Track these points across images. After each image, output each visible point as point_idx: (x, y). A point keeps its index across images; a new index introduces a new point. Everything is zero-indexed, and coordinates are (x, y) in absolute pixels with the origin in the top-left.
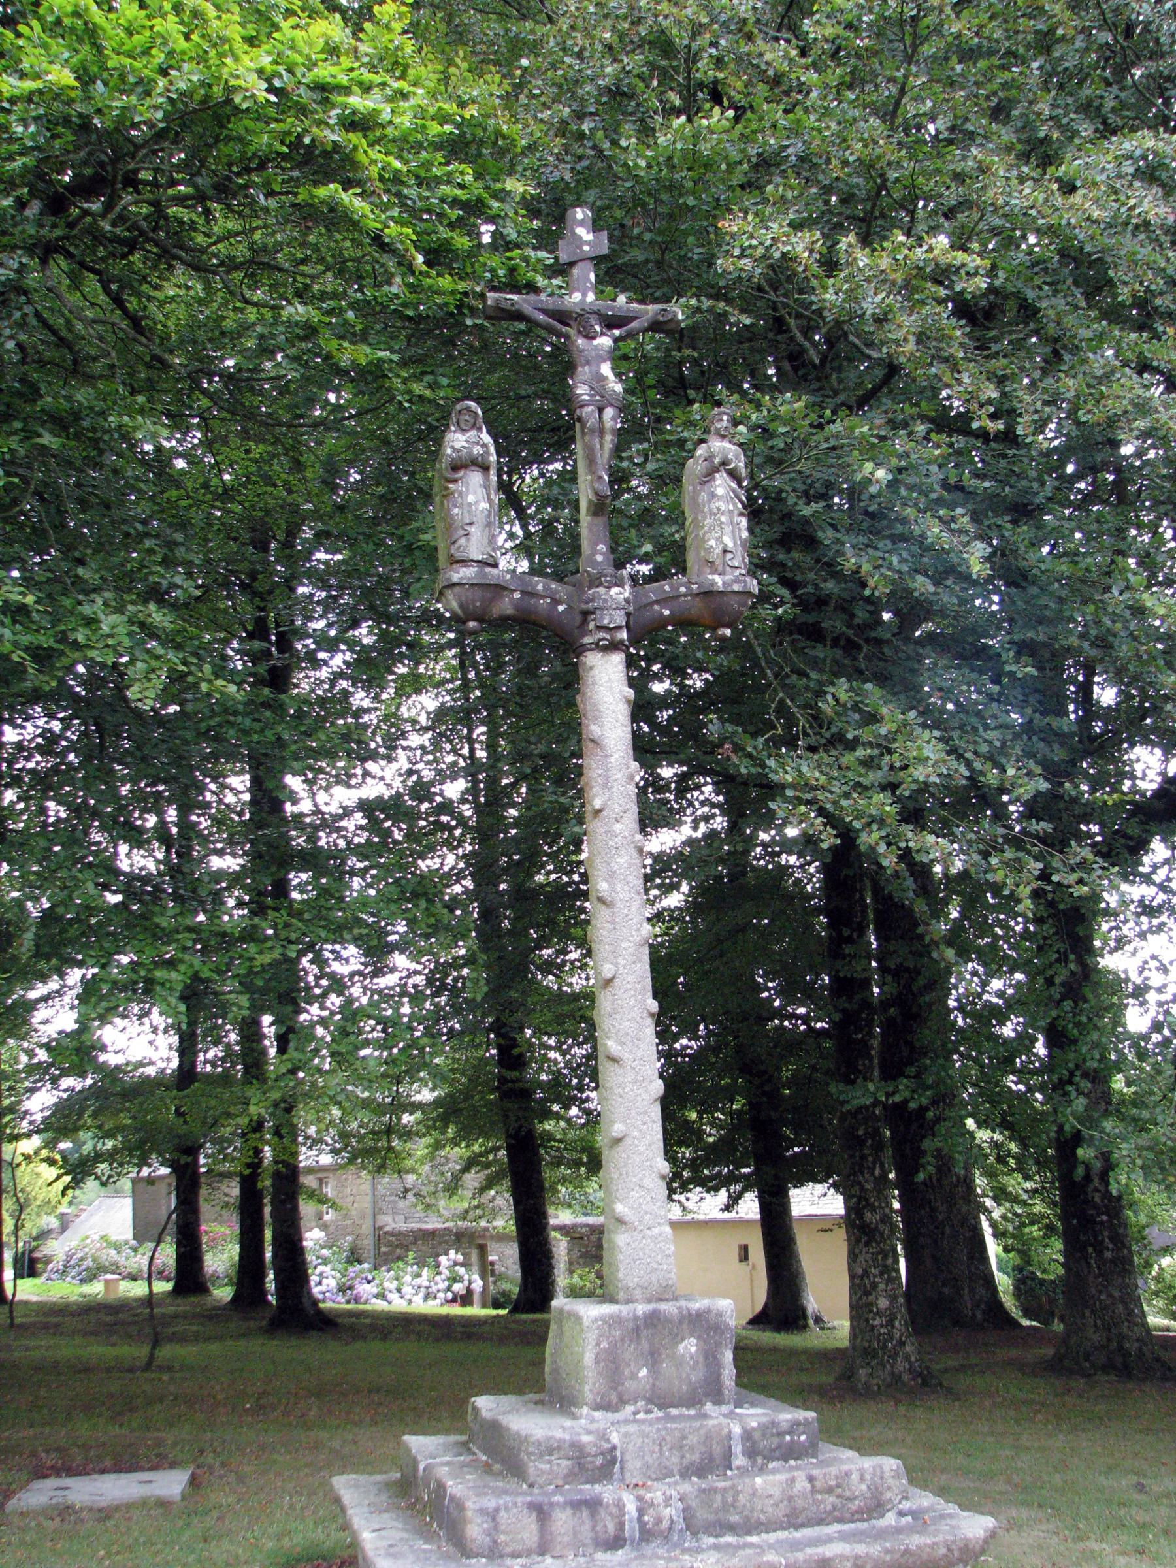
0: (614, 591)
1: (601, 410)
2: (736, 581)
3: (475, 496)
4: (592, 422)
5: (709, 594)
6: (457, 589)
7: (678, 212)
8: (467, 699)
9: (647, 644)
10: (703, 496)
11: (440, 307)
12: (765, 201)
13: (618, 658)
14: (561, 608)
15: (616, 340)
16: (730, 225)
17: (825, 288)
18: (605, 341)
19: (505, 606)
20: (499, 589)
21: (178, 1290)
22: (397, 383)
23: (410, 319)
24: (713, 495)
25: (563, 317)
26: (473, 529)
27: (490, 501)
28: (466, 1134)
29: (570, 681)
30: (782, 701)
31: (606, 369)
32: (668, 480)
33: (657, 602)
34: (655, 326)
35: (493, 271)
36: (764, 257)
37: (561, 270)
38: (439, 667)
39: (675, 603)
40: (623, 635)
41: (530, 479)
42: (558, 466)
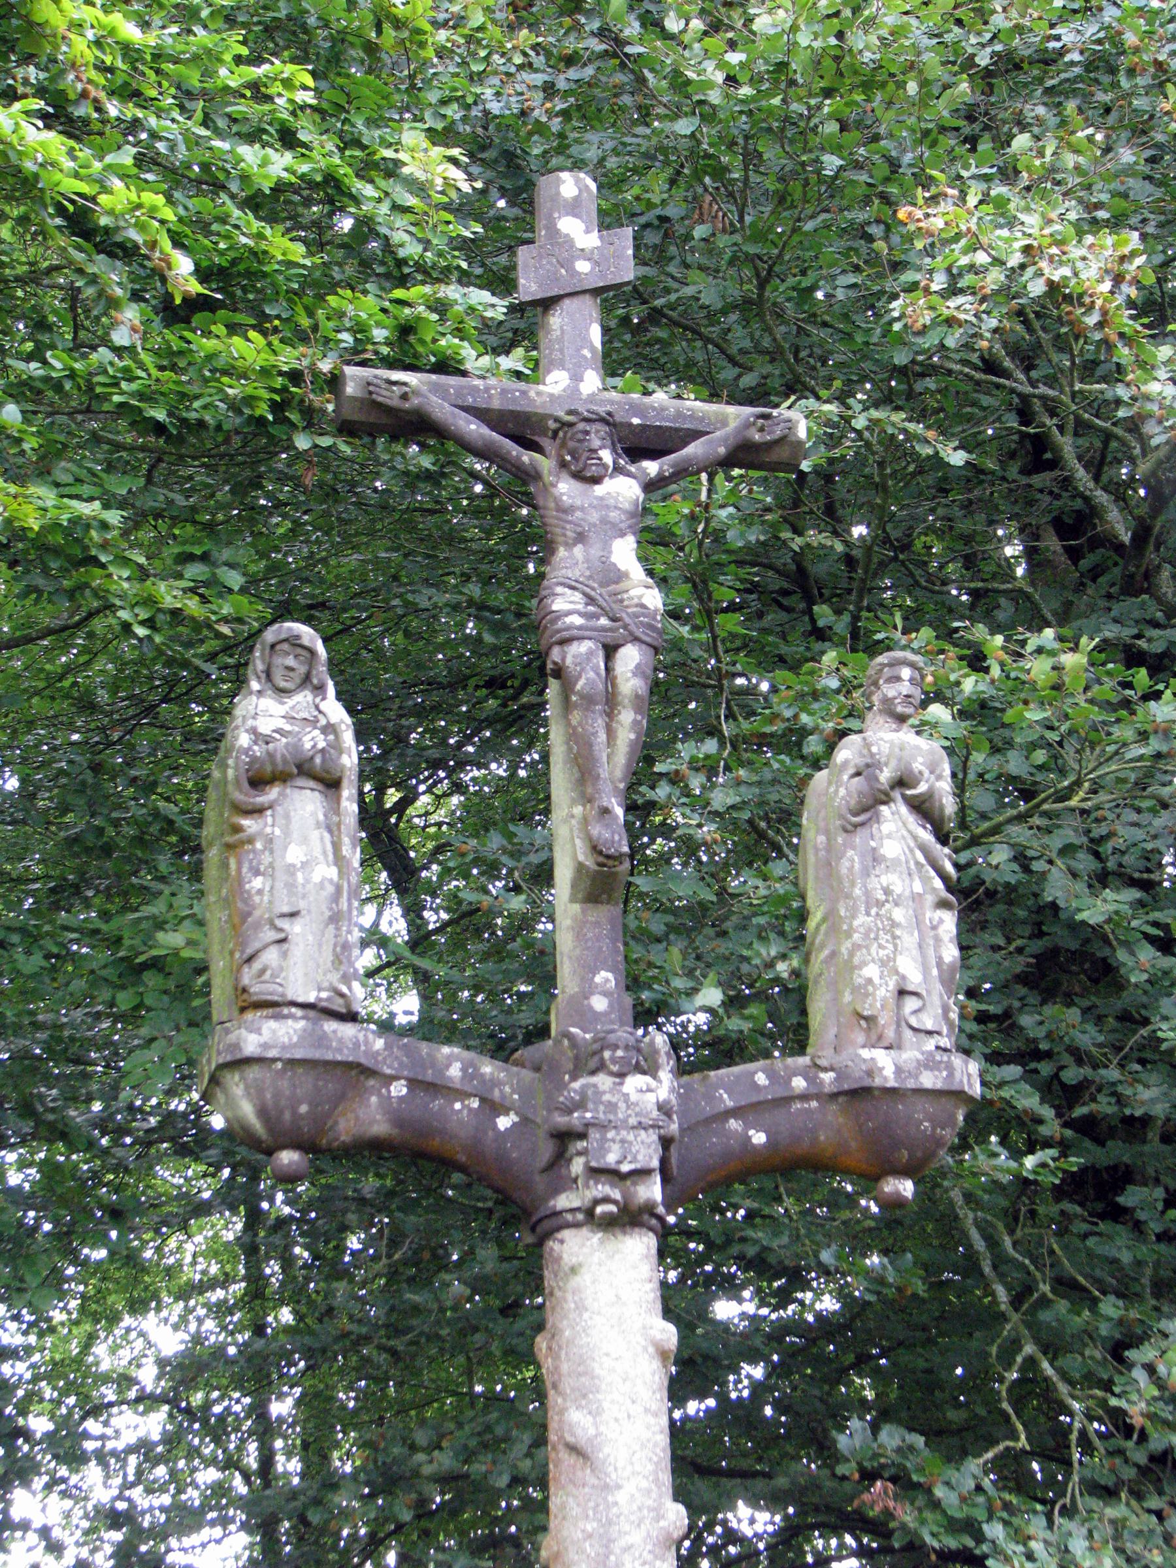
0: (635, 1083)
1: (610, 651)
2: (929, 1064)
3: (302, 852)
4: (588, 679)
5: (860, 1095)
6: (253, 1073)
7: (799, 190)
8: (259, 1330)
9: (714, 1221)
10: (851, 860)
11: (234, 407)
12: (1009, 174)
13: (639, 1246)
14: (504, 1123)
15: (651, 486)
16: (927, 218)
17: (1146, 366)
18: (623, 489)
19: (370, 1115)
20: (358, 1073)
22: (120, 579)
23: (159, 428)
24: (875, 858)
25: (523, 428)
26: (295, 928)
27: (339, 860)
29: (519, 1302)
30: (1031, 1362)
31: (625, 553)
32: (767, 833)
33: (734, 1112)
34: (743, 454)
35: (359, 329)
36: (1006, 292)
37: (522, 328)
38: (190, 1251)
39: (779, 1117)
40: (653, 1191)
41: (431, 810)
42: (499, 770)
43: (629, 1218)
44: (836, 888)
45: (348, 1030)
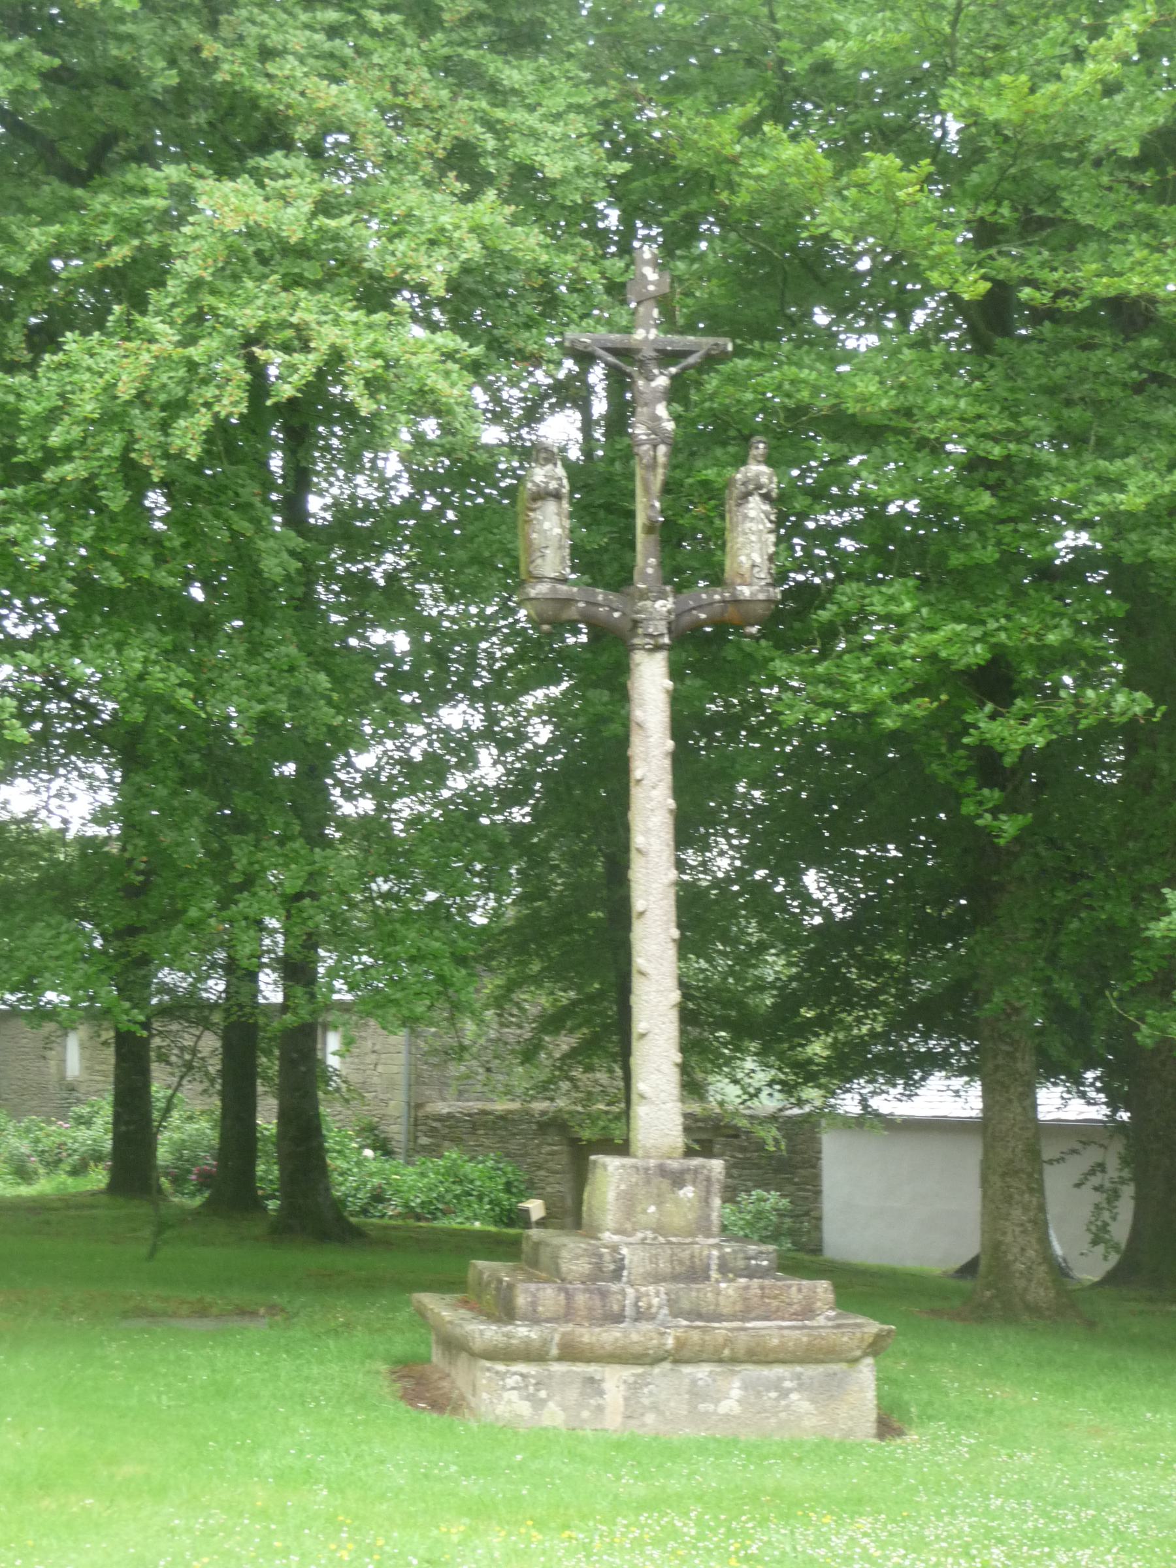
0: (660, 603)
1: (655, 447)
5: (736, 602)
21: (117, 1186)
28: (557, 972)
43: (658, 648)
44: (734, 526)
45: (564, 588)
